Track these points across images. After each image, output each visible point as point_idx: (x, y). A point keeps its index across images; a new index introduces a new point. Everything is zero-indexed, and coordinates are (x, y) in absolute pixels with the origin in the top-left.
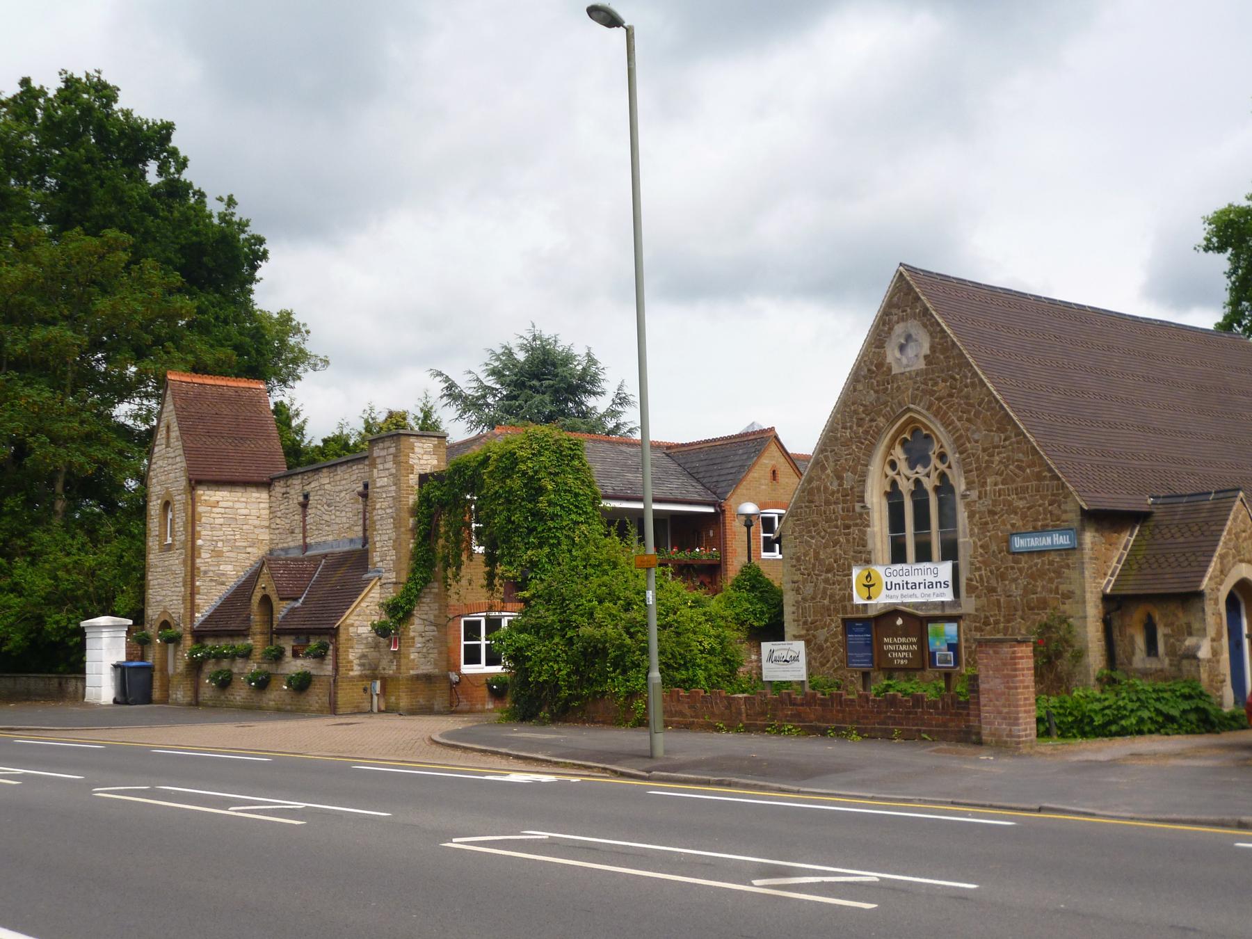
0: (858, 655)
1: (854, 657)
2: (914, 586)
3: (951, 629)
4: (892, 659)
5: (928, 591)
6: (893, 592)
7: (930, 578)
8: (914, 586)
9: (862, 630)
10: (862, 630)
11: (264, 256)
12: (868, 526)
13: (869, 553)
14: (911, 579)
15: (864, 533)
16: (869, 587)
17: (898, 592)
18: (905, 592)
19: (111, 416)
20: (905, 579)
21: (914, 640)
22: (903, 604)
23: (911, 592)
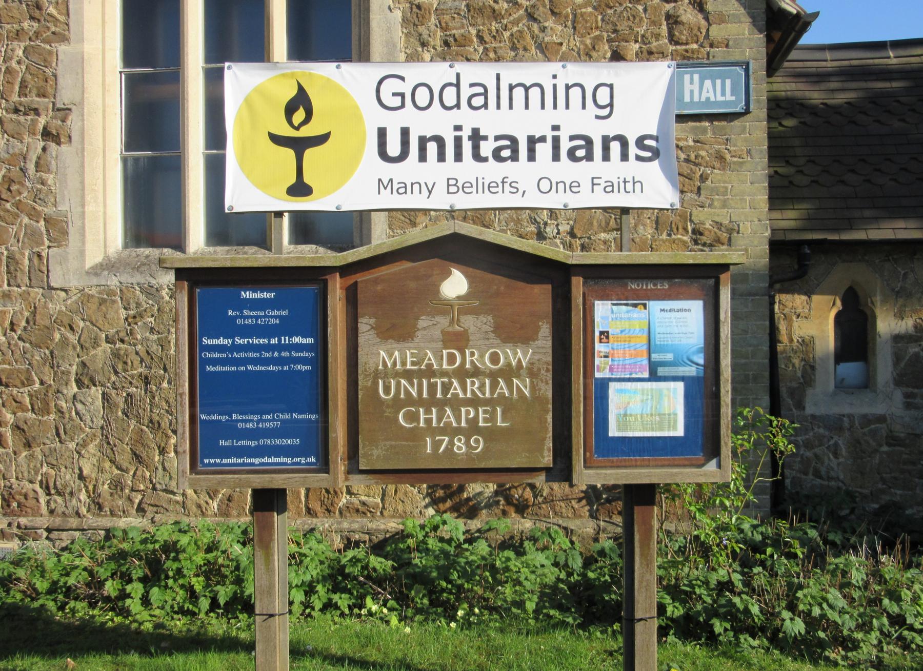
0: (250, 421)
1: (231, 430)
2: (508, 149)
3: (680, 322)
4: (415, 436)
5: (566, 169)
6: (410, 169)
7: (579, 121)
8: (508, 149)
9: (274, 317)
10: (274, 317)
11: (142, 605)
12: (64, 39)
13: (63, 112)
14: (493, 123)
15: (47, 59)
16: (299, 146)
17: (434, 171)
18: (468, 169)
19: (815, 618)
20: (469, 119)
21: (310, 341)
22: (480, 216)
23: (493, 170)
